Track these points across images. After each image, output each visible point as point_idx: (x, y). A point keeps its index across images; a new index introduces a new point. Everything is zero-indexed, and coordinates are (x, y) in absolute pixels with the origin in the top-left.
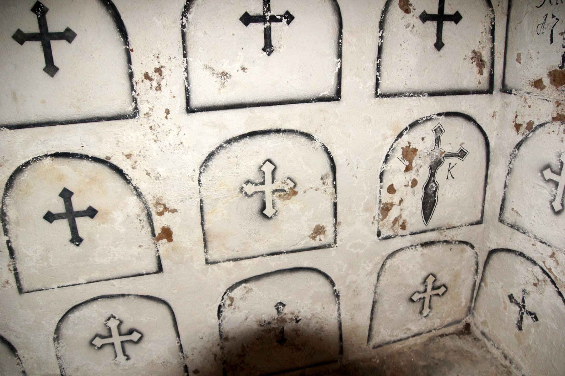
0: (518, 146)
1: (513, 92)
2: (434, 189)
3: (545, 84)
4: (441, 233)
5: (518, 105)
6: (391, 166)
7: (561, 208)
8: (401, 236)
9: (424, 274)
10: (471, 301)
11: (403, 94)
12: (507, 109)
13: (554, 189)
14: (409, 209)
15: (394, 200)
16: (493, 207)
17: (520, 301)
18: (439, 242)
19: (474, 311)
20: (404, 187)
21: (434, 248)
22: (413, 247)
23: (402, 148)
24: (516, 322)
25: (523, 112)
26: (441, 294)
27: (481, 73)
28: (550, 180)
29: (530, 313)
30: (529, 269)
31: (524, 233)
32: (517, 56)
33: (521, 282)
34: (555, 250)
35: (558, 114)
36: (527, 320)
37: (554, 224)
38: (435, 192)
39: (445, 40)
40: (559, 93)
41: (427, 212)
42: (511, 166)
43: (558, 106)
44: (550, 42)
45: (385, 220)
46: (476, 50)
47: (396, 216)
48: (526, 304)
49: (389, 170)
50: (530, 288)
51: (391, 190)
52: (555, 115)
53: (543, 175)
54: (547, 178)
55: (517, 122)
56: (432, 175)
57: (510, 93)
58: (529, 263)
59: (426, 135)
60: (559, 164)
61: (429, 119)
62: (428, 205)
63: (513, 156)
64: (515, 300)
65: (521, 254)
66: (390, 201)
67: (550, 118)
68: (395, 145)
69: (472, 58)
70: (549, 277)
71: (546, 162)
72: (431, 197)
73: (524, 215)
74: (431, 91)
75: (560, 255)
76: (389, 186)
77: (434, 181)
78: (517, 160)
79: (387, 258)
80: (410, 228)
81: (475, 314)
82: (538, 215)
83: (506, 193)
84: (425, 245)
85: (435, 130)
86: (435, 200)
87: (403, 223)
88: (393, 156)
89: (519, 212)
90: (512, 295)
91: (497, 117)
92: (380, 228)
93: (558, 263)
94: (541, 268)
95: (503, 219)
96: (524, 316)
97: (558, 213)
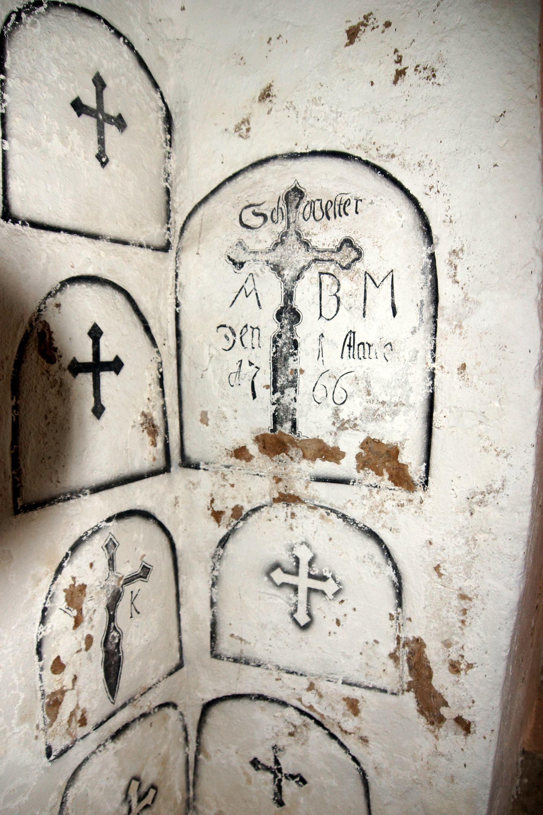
0: (223, 542)
1: (201, 467)
2: (117, 641)
3: (251, 452)
4: (135, 706)
5: (214, 485)
6: (52, 626)
7: (308, 619)
8: (82, 738)
9: (124, 783)
10: (188, 789)
11: (56, 498)
12: (195, 492)
13: (292, 595)
14: (87, 687)
15: (64, 684)
16: (197, 638)
17: (271, 764)
18: (134, 721)
19: (196, 803)
20: (75, 655)
21: (130, 734)
22: (101, 748)
23: (65, 590)
24: (272, 797)
25: (223, 494)
26: (150, 803)
27: (154, 444)
28: (283, 585)
29: (293, 777)
30: (276, 714)
31: (259, 666)
32: (201, 415)
33: (267, 736)
34: (312, 679)
35: (280, 493)
36: (290, 788)
37: (303, 644)
38: (118, 645)
39: (105, 401)
40: (276, 464)
41: (112, 681)
42: (216, 573)
43: (277, 482)
44: (252, 397)
45: (55, 724)
46: (146, 411)
47: (71, 709)
48: (283, 765)
49: (50, 633)
50: (283, 741)
51: (58, 666)
52: (276, 496)
53: (271, 579)
54: (279, 582)
55: (216, 509)
56: (112, 619)
57: (197, 467)
58: (276, 708)
59: (95, 558)
60: (293, 560)
61: (96, 530)
62: (112, 669)
63: (217, 558)
64: (263, 765)
65: (261, 697)
66: (58, 687)
67: (268, 499)
68: (53, 588)
69: (142, 425)
70: (311, 717)
71: (273, 560)
72: (114, 654)
73: (253, 641)
74: (94, 484)
75: (322, 683)
76: (54, 662)
77: (115, 628)
78: (224, 563)
79: (67, 788)
80: (93, 719)
81: (200, 807)
82: (275, 636)
83: (216, 614)
84: (116, 735)
85: (107, 546)
86: (120, 658)
87: (83, 715)
88: (53, 608)
89: (244, 638)
90: (255, 759)
91: (180, 504)
92: (50, 741)
93: (321, 696)
94: (297, 708)
95: (218, 652)
96: (282, 783)
97: (306, 627)
